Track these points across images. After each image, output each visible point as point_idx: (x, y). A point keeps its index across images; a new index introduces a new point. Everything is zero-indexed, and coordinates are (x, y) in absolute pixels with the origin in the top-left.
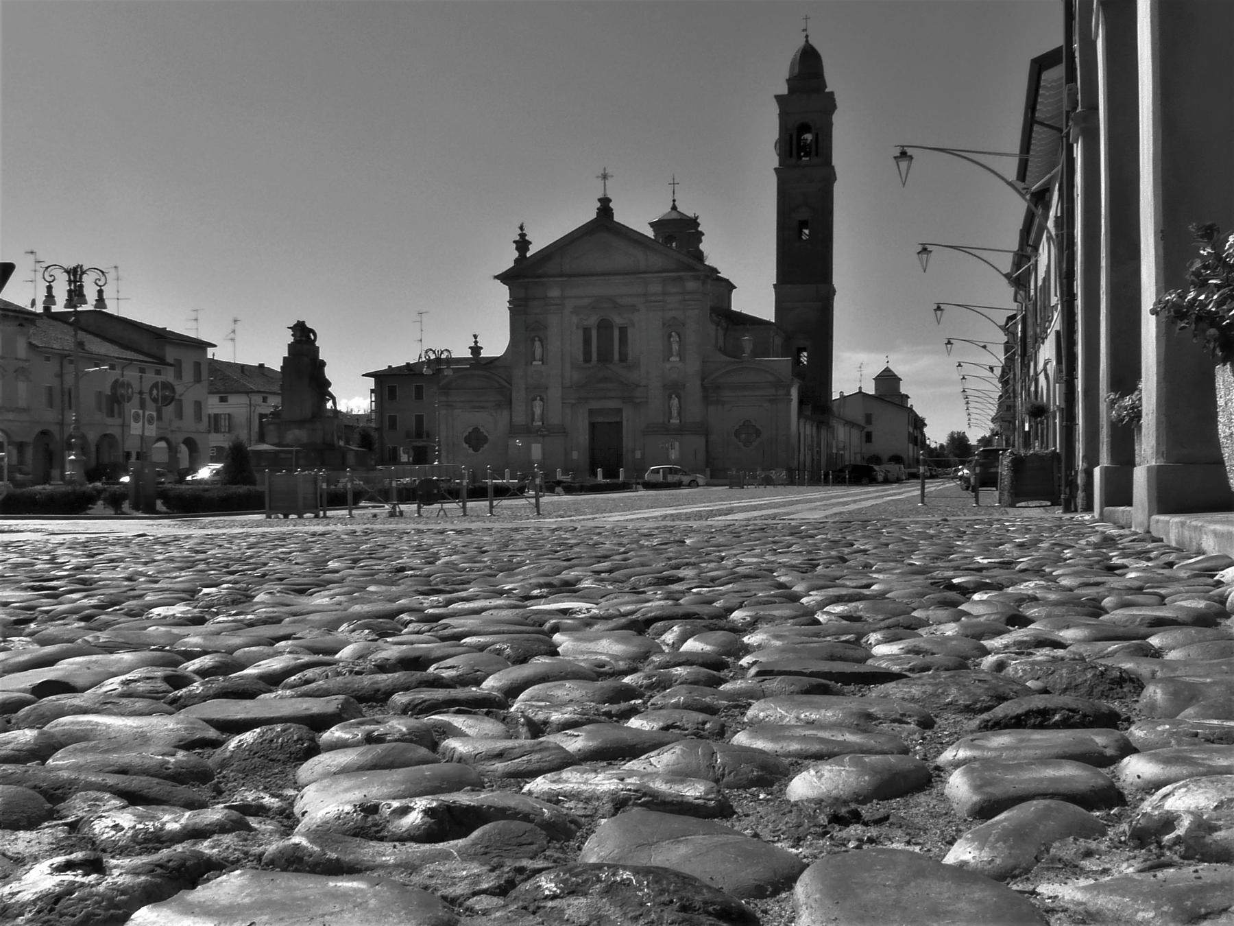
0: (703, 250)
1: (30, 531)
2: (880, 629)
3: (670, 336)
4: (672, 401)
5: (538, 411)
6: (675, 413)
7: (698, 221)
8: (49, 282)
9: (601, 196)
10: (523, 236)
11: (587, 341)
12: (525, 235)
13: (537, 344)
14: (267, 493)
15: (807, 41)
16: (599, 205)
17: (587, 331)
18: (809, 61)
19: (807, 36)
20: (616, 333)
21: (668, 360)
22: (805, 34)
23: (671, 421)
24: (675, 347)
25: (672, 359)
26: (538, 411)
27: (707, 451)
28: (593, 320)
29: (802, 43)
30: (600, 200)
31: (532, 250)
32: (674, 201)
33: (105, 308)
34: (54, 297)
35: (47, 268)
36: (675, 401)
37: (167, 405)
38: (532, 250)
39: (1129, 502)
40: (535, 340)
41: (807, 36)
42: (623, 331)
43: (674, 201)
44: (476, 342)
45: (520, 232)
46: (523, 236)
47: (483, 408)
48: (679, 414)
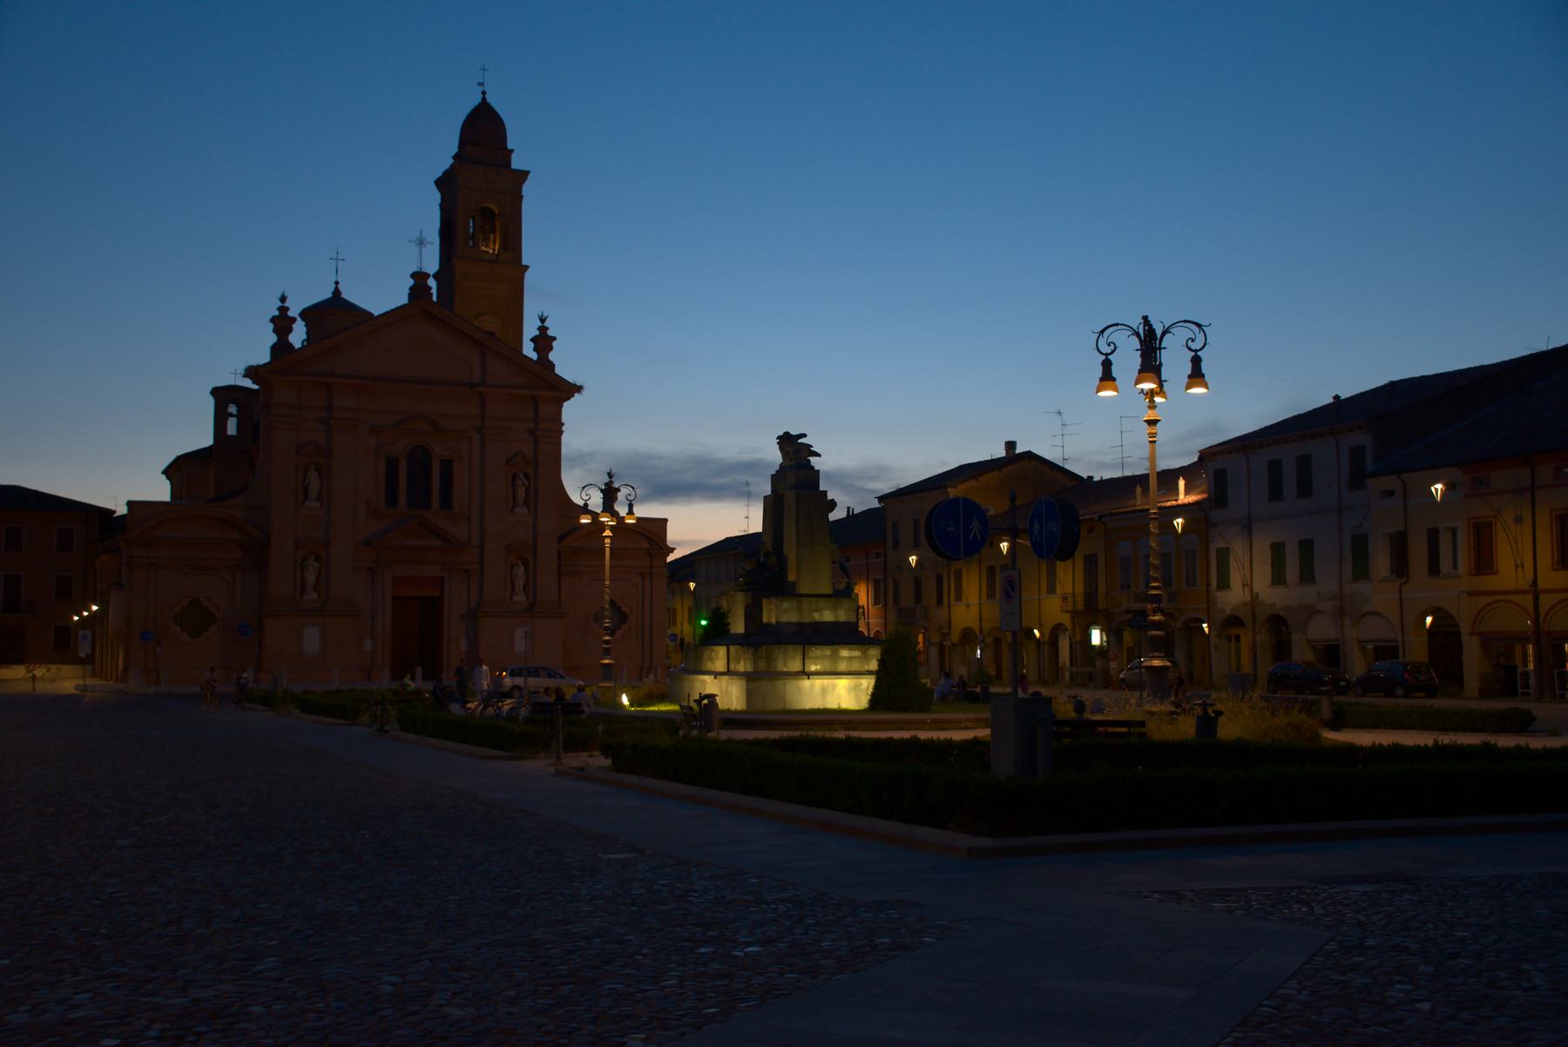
1: (307, 704)
2: (1255, 670)
3: (515, 477)
5: (311, 577)
6: (520, 583)
8: (1107, 355)
9: (415, 269)
12: (547, 329)
13: (313, 475)
14: (1400, 645)
15: (484, 99)
16: (411, 282)
17: (392, 464)
19: (484, 93)
21: (512, 511)
22: (480, 89)
24: (521, 493)
25: (517, 510)
26: (311, 577)
27: (1251, 543)
29: (479, 99)
30: (414, 275)
32: (337, 283)
35: (1102, 332)
41: (484, 93)
42: (447, 465)
43: (337, 283)
45: (540, 324)
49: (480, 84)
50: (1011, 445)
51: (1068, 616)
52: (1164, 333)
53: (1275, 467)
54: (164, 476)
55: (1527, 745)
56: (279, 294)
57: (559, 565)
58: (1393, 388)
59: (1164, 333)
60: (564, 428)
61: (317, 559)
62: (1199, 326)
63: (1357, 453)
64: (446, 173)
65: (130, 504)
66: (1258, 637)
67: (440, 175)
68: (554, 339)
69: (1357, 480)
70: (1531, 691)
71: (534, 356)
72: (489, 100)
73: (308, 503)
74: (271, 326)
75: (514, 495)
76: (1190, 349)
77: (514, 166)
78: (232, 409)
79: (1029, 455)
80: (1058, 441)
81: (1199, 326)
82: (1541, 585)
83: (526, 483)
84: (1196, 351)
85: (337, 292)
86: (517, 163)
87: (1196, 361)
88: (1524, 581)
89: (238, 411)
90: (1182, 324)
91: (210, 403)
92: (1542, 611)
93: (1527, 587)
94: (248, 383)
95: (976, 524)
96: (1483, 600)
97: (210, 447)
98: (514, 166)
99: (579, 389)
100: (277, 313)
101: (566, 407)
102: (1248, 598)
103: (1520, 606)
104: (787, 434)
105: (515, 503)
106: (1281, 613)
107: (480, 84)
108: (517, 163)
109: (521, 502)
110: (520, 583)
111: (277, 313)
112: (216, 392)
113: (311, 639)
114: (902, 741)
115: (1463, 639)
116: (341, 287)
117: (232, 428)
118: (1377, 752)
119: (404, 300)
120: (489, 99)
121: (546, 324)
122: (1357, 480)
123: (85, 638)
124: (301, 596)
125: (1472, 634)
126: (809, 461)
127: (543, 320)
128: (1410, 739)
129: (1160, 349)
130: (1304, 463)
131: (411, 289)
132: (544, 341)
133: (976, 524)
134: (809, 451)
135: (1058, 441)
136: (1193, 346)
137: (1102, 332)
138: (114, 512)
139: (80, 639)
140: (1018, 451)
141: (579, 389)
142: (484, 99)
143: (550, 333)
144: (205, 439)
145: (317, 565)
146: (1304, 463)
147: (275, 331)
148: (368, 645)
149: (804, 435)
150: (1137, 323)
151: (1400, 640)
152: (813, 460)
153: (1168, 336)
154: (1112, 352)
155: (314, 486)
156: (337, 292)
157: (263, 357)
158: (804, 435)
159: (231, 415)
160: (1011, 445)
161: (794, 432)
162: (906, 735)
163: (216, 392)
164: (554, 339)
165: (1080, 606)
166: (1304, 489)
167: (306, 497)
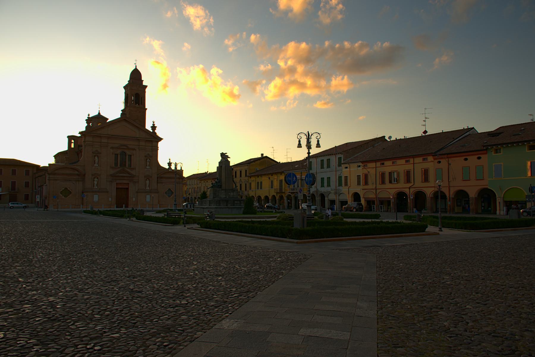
0: (85, 128)
4: (147, 182)
5: (96, 183)
6: (148, 185)
7: (156, 128)
8: (299, 139)
10: (154, 125)
11: (116, 159)
12: (155, 124)
13: (96, 158)
14: (336, 200)
15: (136, 68)
18: (136, 75)
19: (136, 66)
20: (127, 156)
22: (135, 65)
23: (146, 188)
24: (148, 163)
26: (96, 183)
28: (119, 152)
31: (310, 155)
32: (99, 111)
33: (108, 119)
34: (301, 144)
35: (299, 134)
36: (148, 182)
37: (530, 188)
38: (310, 155)
39: (117, 207)
40: (95, 157)
41: (136, 66)
43: (99, 111)
44: (170, 161)
45: (153, 123)
46: (154, 125)
47: (70, 180)
48: (149, 186)
49: (135, 64)
50: (262, 155)
51: (276, 193)
52: (311, 135)
53: (322, 161)
54: (54, 157)
55: (388, 221)
56: (88, 114)
57: (157, 181)
58: (346, 144)
59: (311, 135)
60: (159, 148)
61: (98, 178)
62: (319, 134)
63: (340, 159)
64: (127, 85)
65: (49, 164)
66: (318, 198)
67: (125, 85)
68: (156, 127)
69: (340, 165)
70: (375, 210)
71: (151, 131)
72: (137, 68)
73: (95, 165)
74: (86, 121)
75: (146, 164)
76: (317, 138)
77: (144, 84)
78: (73, 141)
79: (266, 157)
80: (272, 154)
81: (319, 134)
82: (377, 188)
83: (149, 161)
84: (318, 139)
85: (99, 113)
86: (144, 84)
87: (318, 141)
88: (374, 187)
89: (74, 142)
90: (317, 134)
91: (67, 140)
92: (377, 193)
93: (374, 188)
94: (79, 135)
95: (294, 178)
96: (366, 191)
97: (67, 150)
98: (144, 84)
99: (162, 139)
100: (87, 119)
101: (159, 143)
102: (316, 190)
103: (372, 192)
104: (222, 153)
105: (147, 166)
106: (323, 193)
107: (135, 64)
108: (144, 84)
109: (148, 166)
110: (148, 185)
111: (87, 119)
112: (68, 137)
113: (96, 198)
114: (263, 221)
115: (361, 199)
116: (100, 112)
117: (73, 146)
118: (352, 223)
119: (120, 117)
120: (138, 68)
121: (154, 123)
122: (340, 165)
123: (38, 197)
124: (93, 187)
125: (363, 198)
126: (228, 159)
127: (154, 122)
128: (357, 220)
129: (311, 138)
130: (328, 160)
131: (121, 114)
132: (154, 127)
133: (294, 178)
134: (228, 157)
135: (272, 154)
136: (318, 138)
137: (299, 134)
138: (40, 166)
139: (37, 198)
140: (264, 156)
141: (162, 139)
142: (136, 68)
143: (155, 126)
144: (66, 148)
145: (97, 180)
146: (328, 160)
147: (87, 123)
148: (110, 199)
149: (227, 153)
150: (306, 132)
151: (348, 199)
152: (229, 159)
153: (312, 136)
154: (301, 139)
155: (97, 161)
156: (99, 113)
157: (84, 129)
158: (227, 153)
159: (73, 143)
160: (262, 155)
161: (224, 153)
162: (264, 220)
163: (68, 137)
164: (156, 127)
165: (278, 191)
166: (329, 166)
167: (95, 163)
